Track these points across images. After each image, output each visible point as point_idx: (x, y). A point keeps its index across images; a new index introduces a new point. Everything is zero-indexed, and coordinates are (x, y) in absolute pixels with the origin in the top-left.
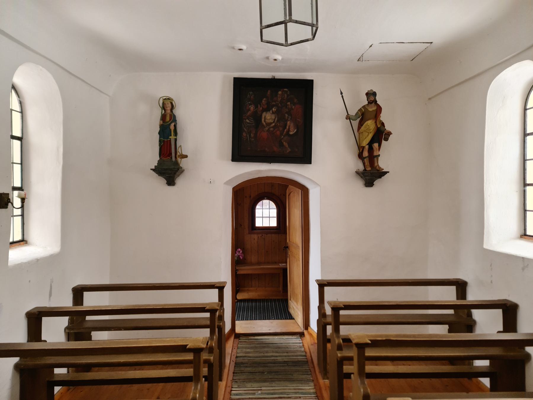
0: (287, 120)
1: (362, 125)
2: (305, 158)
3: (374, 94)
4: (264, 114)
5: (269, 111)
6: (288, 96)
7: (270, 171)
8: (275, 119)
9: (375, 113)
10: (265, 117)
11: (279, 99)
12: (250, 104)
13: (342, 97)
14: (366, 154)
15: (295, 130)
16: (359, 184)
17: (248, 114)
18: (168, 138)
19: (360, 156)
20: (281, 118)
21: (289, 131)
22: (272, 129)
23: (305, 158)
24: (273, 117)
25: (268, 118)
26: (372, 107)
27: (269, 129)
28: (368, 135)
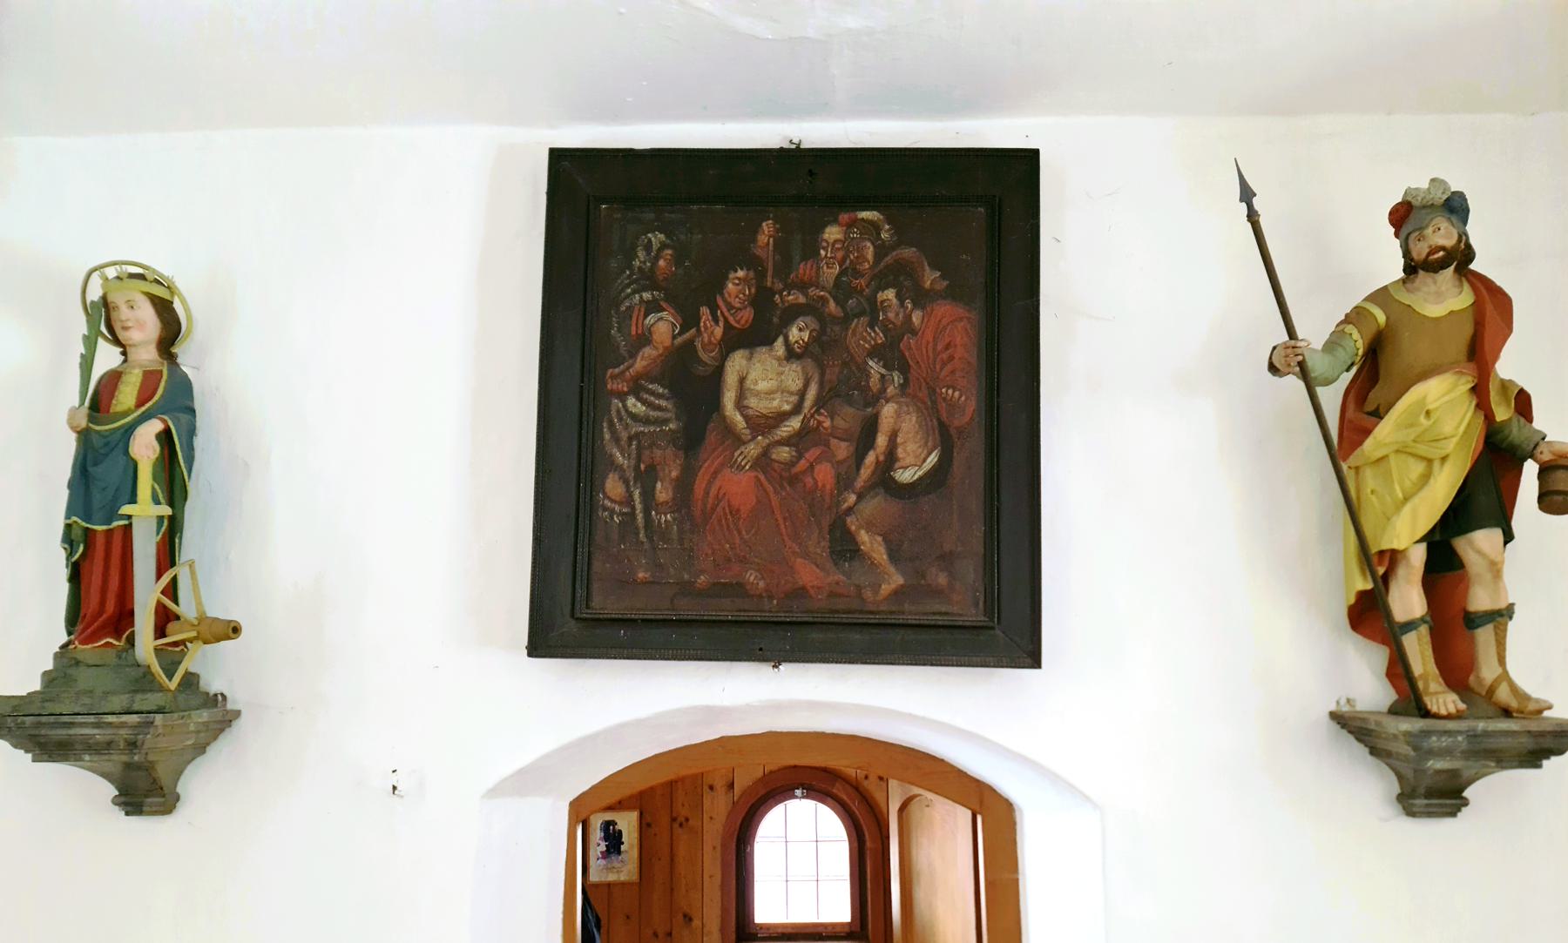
0: (876, 399)
1: (1378, 415)
2: (999, 623)
3: (1456, 207)
4: (736, 363)
5: (769, 342)
6: (879, 256)
7: (778, 707)
8: (802, 394)
9: (1468, 330)
10: (742, 380)
11: (830, 273)
12: (652, 307)
13: (1253, 217)
14: (1408, 600)
15: (933, 459)
16: (1367, 788)
17: (640, 364)
18: (112, 515)
19: (1368, 614)
20: (841, 387)
21: (891, 459)
22: (784, 453)
23: (999, 623)
24: (793, 376)
25: (763, 386)
26: (1439, 297)
27: (765, 453)
28: (1426, 478)
